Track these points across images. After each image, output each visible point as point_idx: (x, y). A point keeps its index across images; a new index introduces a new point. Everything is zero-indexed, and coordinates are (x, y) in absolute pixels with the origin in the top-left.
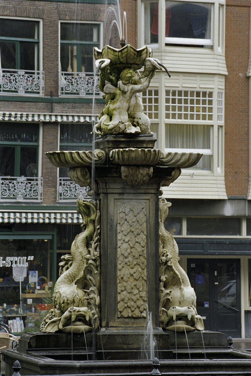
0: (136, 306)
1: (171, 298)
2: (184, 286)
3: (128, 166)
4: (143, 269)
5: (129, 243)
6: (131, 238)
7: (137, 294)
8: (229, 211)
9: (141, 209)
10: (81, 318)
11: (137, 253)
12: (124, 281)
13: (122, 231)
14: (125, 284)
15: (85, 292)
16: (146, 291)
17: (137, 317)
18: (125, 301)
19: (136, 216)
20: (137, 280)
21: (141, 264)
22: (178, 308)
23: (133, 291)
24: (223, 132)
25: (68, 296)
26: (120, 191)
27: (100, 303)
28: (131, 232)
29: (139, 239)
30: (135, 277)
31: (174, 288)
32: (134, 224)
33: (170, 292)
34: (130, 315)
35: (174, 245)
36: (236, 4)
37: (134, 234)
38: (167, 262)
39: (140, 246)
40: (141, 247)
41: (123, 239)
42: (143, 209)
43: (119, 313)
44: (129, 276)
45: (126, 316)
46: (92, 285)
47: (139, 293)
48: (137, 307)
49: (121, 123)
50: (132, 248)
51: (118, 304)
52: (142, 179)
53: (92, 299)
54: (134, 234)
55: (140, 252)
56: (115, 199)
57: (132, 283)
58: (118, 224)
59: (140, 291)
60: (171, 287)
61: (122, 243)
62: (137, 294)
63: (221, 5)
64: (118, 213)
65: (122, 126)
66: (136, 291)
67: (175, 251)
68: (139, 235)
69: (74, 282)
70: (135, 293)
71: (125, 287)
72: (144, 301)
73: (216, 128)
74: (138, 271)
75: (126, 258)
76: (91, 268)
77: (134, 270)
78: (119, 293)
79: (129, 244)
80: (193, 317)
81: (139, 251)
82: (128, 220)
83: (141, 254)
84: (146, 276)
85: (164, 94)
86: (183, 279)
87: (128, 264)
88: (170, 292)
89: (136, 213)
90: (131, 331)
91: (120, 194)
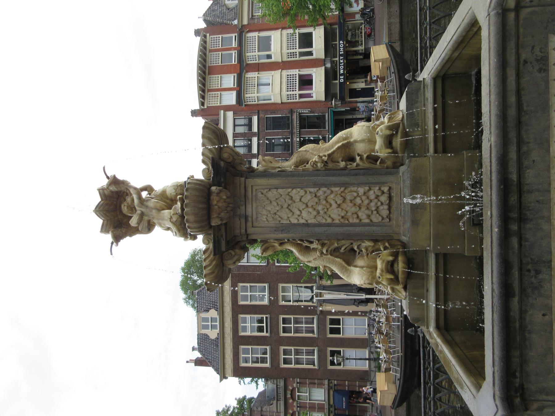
0: (376, 200)
5: (301, 209)
6: (296, 208)
7: (361, 198)
8: (329, 65)
9: (263, 195)
10: (391, 267)
12: (346, 215)
13: (288, 218)
14: (349, 214)
15: (359, 253)
16: (358, 188)
17: (389, 199)
18: (370, 213)
19: (271, 202)
21: (326, 195)
22: (377, 147)
23: (357, 204)
24: (301, 70)
26: (243, 221)
27: (372, 240)
28: (290, 207)
29: (297, 198)
30: (341, 202)
32: (279, 203)
33: (359, 155)
34: (386, 207)
35: (305, 151)
37: (291, 203)
38: (323, 161)
39: (305, 196)
40: (307, 195)
41: (297, 216)
42: (262, 194)
43: (384, 221)
44: (340, 209)
45: (388, 212)
46: (351, 246)
47: (359, 197)
48: (376, 198)
50: (307, 206)
51: (374, 221)
52: (225, 199)
53: (367, 249)
54: (291, 203)
55: (311, 196)
56: (253, 227)
57: (348, 206)
58: (281, 222)
59: (358, 195)
61: (302, 218)
62: (361, 198)
63: (258, 73)
65: (174, 219)
66: (358, 201)
67: (312, 149)
68: (292, 197)
71: (353, 214)
73: (299, 72)
74: (334, 199)
76: (331, 251)
77: (333, 202)
78: (361, 220)
80: (390, 128)
81: (311, 197)
82: (276, 211)
83: (314, 195)
84: (339, 188)
87: (326, 210)
88: (359, 155)
89: (267, 202)
91: (246, 221)
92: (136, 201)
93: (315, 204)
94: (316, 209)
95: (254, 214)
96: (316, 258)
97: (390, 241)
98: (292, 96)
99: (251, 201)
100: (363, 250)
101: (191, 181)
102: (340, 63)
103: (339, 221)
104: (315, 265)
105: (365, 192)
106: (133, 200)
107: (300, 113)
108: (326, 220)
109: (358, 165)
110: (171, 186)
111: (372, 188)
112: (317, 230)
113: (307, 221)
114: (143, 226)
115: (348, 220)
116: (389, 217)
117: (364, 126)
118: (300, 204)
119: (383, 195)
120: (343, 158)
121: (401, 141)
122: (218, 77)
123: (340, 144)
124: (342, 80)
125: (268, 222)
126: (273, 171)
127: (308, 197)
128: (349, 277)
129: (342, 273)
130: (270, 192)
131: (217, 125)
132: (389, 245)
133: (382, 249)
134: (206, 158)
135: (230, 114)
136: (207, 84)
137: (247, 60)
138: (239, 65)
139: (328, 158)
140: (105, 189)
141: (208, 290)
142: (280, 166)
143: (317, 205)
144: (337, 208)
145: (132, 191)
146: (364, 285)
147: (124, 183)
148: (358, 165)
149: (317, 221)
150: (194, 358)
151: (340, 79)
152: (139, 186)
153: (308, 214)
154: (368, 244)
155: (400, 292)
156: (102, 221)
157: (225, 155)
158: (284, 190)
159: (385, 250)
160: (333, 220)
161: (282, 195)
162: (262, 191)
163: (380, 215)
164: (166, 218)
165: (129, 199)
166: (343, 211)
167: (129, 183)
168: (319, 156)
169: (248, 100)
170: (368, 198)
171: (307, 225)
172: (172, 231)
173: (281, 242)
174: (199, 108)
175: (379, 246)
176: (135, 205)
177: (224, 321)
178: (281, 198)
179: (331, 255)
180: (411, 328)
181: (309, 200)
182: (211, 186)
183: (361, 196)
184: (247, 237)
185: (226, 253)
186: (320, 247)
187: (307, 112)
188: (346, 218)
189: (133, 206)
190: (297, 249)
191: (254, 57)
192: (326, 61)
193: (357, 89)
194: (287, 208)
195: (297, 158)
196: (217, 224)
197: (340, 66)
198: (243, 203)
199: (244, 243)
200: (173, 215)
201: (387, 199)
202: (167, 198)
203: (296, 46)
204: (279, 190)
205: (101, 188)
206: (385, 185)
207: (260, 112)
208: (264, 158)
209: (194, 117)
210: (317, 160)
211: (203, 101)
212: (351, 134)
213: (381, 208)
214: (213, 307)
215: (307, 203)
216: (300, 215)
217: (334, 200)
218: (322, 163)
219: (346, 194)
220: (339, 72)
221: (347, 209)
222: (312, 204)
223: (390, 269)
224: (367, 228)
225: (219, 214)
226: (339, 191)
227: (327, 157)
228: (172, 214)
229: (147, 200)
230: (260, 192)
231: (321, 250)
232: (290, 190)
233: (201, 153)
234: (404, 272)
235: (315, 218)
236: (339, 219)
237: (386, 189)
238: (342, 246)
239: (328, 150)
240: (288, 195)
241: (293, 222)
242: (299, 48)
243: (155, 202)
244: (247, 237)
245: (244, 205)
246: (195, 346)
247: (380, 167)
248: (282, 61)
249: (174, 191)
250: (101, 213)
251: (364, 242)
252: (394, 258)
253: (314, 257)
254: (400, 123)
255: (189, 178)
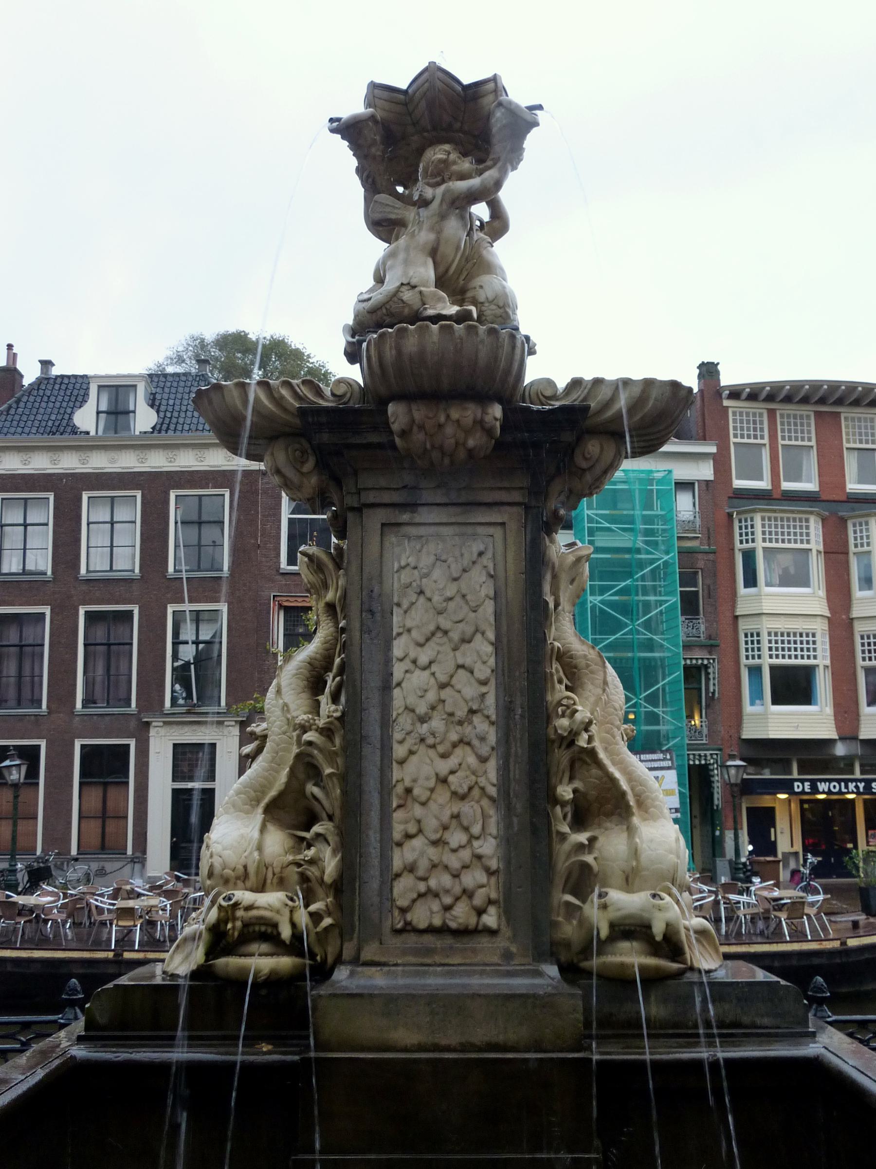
1: (595, 859)
2: (645, 820)
3: (403, 397)
4: (483, 760)
5: (434, 668)
6: (438, 652)
7: (463, 847)
8: (840, 750)
9: (475, 555)
11: (463, 704)
12: (415, 800)
13: (409, 631)
14: (418, 811)
15: (302, 839)
16: (495, 838)
17: (462, 927)
18: (421, 872)
19: (455, 579)
20: (463, 798)
21: (476, 742)
23: (447, 836)
25: (227, 853)
28: (439, 634)
29: (466, 656)
30: (453, 788)
31: (608, 825)
32: (452, 605)
33: (592, 840)
34: (437, 922)
35: (605, 683)
36: (832, 499)
37: (450, 640)
39: (473, 681)
40: (476, 684)
41: (412, 655)
42: (481, 554)
43: (396, 913)
44: (432, 783)
45: (423, 925)
46: (324, 815)
47: (469, 842)
48: (464, 891)
49: (406, 288)
50: (443, 686)
51: (395, 884)
52: (464, 444)
53: (312, 862)
54: (450, 640)
55: (472, 699)
57: (442, 806)
59: (472, 837)
60: (596, 821)
61: (407, 671)
62: (463, 847)
63: (819, 552)
64: (395, 570)
65: (407, 295)
66: (457, 838)
69: (263, 804)
70: (454, 844)
71: (419, 822)
72: (490, 873)
73: (821, 668)
75: (423, 720)
76: (310, 755)
77: (453, 762)
79: (433, 674)
82: (428, 594)
83: (475, 708)
84: (495, 781)
85: (766, 634)
86: (638, 797)
87: (430, 741)
88: (592, 840)
89: (455, 571)
90: (440, 981)
92: (462, 185)
93: (449, 709)
94: (435, 713)
95: (422, 531)
96: (288, 711)
97: (336, 931)
98: (756, 645)
99: (460, 519)
100: (311, 853)
101: (519, 344)
102: (846, 781)
103: (398, 781)
104: (269, 709)
105: (483, 860)
106: (463, 177)
107: (706, 667)
108: (401, 742)
109: (563, 837)
110: (504, 287)
111: (493, 880)
112: (373, 714)
113: (399, 684)
114: (387, 205)
115: (399, 806)
116: (409, 928)
117: (678, 857)
118: (450, 666)
119: (474, 913)
120: (584, 795)
121: (633, 966)
122: (810, 440)
123: (624, 785)
124: (798, 787)
125: (397, 572)
126: (547, 588)
127: (470, 691)
128: (232, 810)
129: (245, 787)
130: (484, 578)
131: (678, 437)
132: (326, 929)
133: (313, 908)
134: (586, 391)
135: (705, 472)
136: (790, 409)
137: (857, 521)
138: (844, 498)
139: (583, 748)
140: (497, 96)
141: (199, 393)
142: (560, 608)
143: (445, 716)
144: (437, 775)
145: (491, 174)
146: (208, 853)
147: (515, 155)
148: (563, 837)
149: (399, 714)
150: (20, 366)
151: (802, 781)
152: (504, 195)
153: (420, 689)
154: (331, 865)
155: (187, 957)
156: (404, 86)
157: (593, 447)
158: (492, 619)
159: (311, 914)
160: (401, 763)
161: (475, 611)
162: (489, 554)
163: (414, 901)
164: (411, 273)
165: (466, 165)
166: (428, 793)
167: (514, 168)
168: (590, 723)
169: (746, 521)
170: (465, 867)
171: (387, 686)
172: (371, 290)
173: (338, 610)
174: (723, 384)
175: (323, 900)
176: (451, 183)
177: (123, 451)
178: (466, 609)
179: (298, 756)
180: (83, 988)
181: (459, 692)
182: (506, 401)
183: (472, 846)
184: (352, 509)
185: (306, 445)
186: (321, 722)
187: (711, 690)
188: (406, 800)
189: (446, 177)
190: (318, 656)
191: (865, 540)
192: (854, 742)
193: (772, 830)
194: (438, 628)
195: (585, 656)
196: (392, 420)
197: (839, 781)
198: (453, 497)
199: (335, 498)
200: (421, 292)
201: (460, 924)
202: (470, 277)
203: (777, 656)
204: (492, 602)
205: (499, 85)
206: (503, 919)
207: (711, 557)
208: (584, 560)
209: (698, 371)
210: (578, 716)
211: (744, 396)
212: (654, 818)
213: (436, 906)
214: (164, 419)
215: (452, 686)
216: (416, 666)
217: (460, 765)
218: (570, 732)
219: (478, 802)
220: (821, 780)
221: (431, 804)
222: (449, 701)
223: (254, 931)
224: (376, 862)
225: (421, 427)
226: (487, 779)
227: (586, 746)
228: (422, 289)
229: (466, 218)
230: (486, 549)
231: (314, 727)
232: (491, 635)
233: (600, 376)
234: (245, 971)
235: (406, 708)
236: (403, 780)
237: (490, 919)
238: (323, 788)
239: (606, 749)
240: (477, 631)
241: (395, 643)
242: (773, 668)
243: (460, 240)
244: (352, 509)
245: (447, 501)
246: (54, 368)
247: (555, 903)
248: (852, 619)
249: (490, 296)
250: (427, 85)
251: (334, 852)
252: (288, 942)
253: (292, 706)
254: (684, 962)
255: (527, 338)
